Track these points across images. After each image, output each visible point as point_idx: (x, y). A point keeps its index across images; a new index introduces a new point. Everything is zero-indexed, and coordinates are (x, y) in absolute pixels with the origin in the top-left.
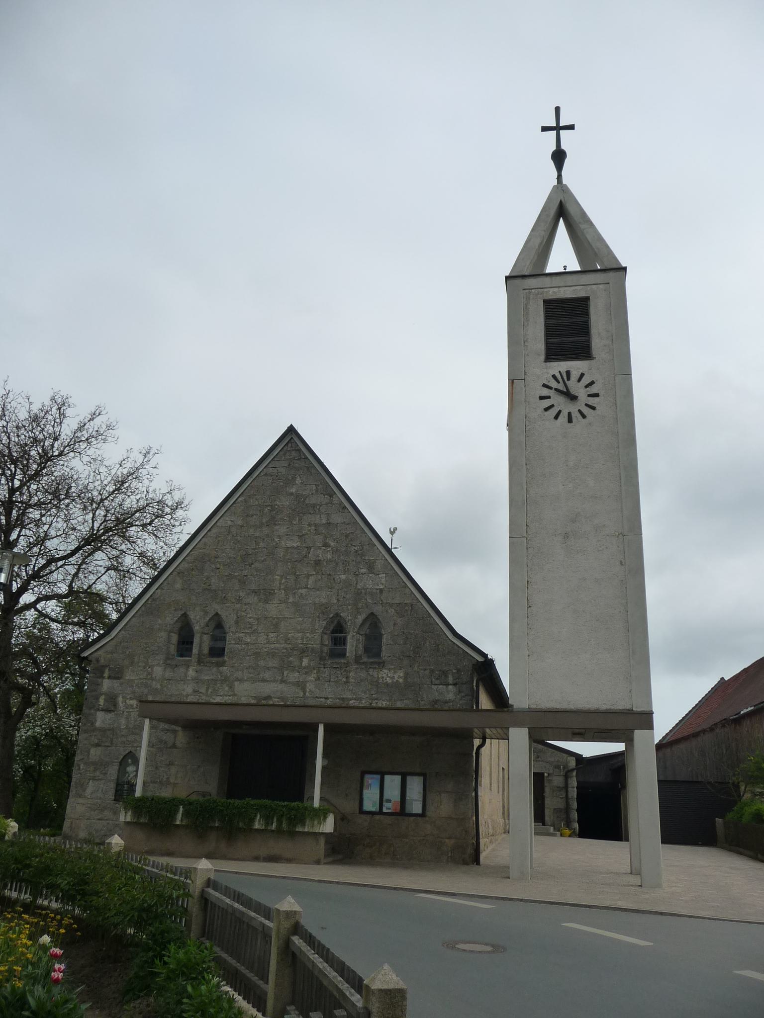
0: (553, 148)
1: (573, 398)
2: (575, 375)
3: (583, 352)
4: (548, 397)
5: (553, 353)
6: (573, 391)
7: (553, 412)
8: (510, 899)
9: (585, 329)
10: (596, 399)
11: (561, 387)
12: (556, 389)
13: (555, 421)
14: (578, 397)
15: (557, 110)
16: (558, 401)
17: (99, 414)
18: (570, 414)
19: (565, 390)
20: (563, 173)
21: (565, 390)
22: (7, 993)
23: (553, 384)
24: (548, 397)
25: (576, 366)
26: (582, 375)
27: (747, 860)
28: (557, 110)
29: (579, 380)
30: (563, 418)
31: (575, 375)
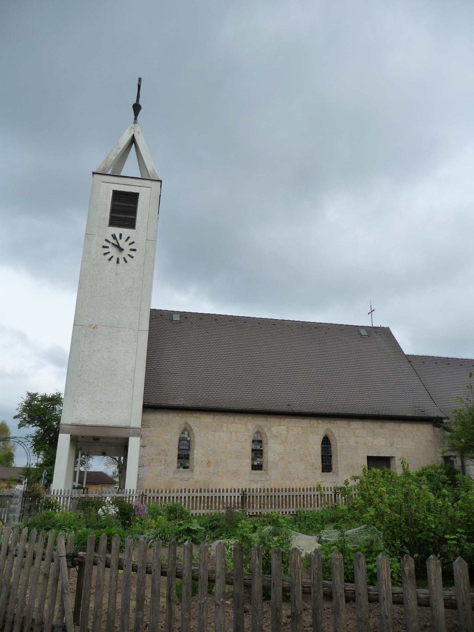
0: (135, 102)
1: (121, 250)
2: (124, 237)
3: (131, 224)
4: (107, 247)
5: (114, 222)
6: (121, 246)
7: (109, 256)
8: (161, 187)
9: (134, 212)
10: (131, 259)
11: (115, 242)
12: (112, 243)
13: (109, 261)
14: (124, 249)
15: (140, 80)
16: (113, 251)
17: (120, 551)
18: (118, 259)
19: (117, 244)
20: (138, 118)
21: (117, 244)
22: (258, 453)
23: (112, 240)
24: (107, 247)
25: (126, 232)
26: (129, 238)
27: (165, 413)
28: (140, 80)
29: (126, 240)
30: (114, 260)
31: (124, 237)
